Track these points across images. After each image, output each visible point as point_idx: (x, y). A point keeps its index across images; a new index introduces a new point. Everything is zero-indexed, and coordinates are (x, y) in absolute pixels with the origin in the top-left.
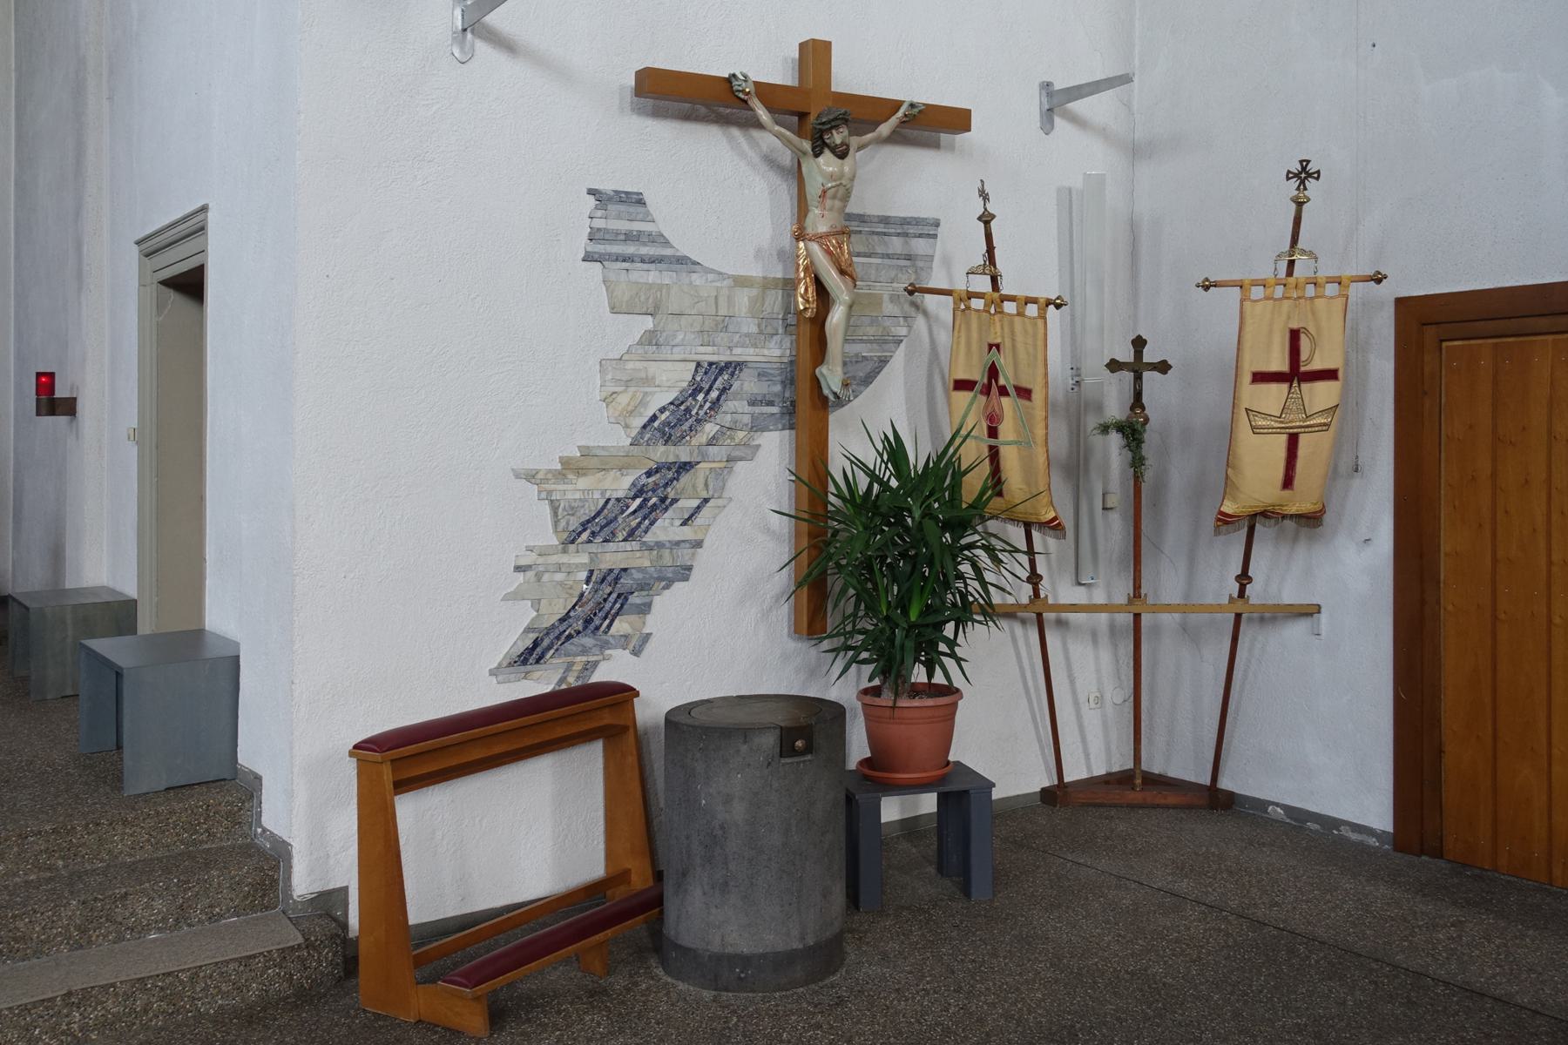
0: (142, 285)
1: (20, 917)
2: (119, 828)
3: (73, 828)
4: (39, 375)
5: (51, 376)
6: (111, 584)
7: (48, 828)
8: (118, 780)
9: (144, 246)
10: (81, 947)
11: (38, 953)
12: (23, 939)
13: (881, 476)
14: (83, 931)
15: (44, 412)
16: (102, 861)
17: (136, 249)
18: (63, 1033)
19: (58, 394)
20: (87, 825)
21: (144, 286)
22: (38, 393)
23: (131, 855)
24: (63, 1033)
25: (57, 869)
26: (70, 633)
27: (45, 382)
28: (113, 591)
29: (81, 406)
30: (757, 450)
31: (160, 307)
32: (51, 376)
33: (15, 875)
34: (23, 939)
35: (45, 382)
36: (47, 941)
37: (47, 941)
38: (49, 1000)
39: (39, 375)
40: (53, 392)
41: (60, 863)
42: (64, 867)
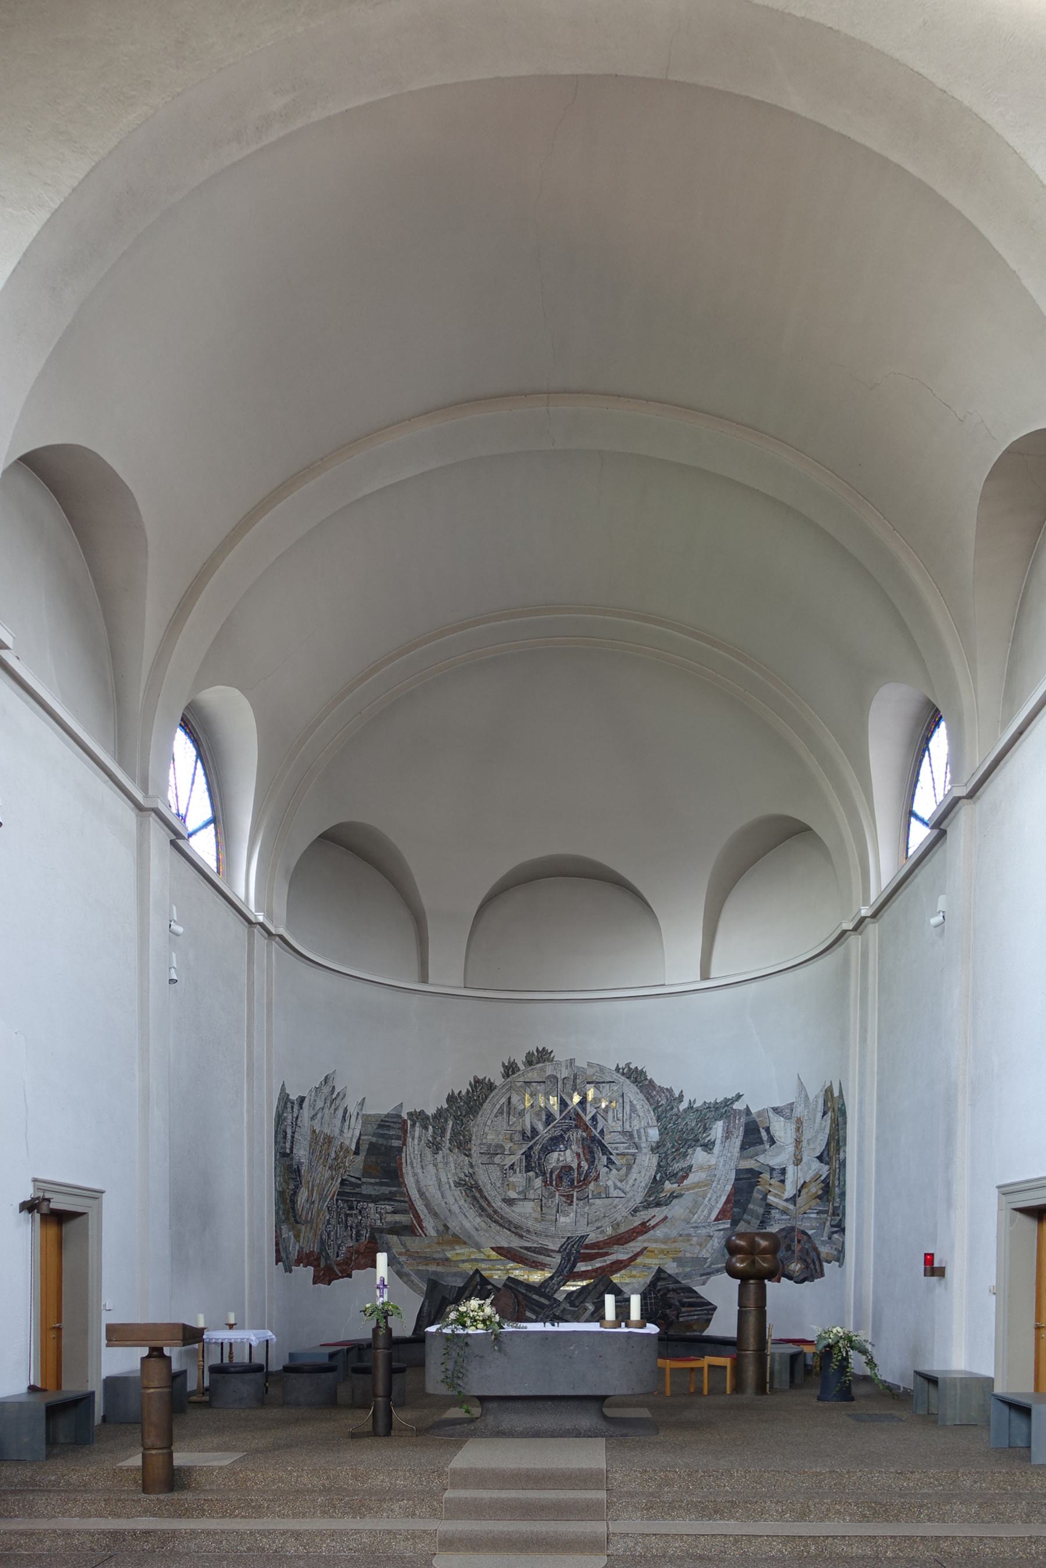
0: (1000, 1209)
1: (1001, 1504)
2: (1036, 1476)
3: (1015, 1473)
4: (926, 1255)
5: (932, 1255)
6: (968, 1369)
7: (1004, 1471)
8: (1028, 1458)
9: (1002, 1189)
10: (1026, 1523)
11: (1008, 1522)
12: (1002, 1514)
13: (681, 1315)
14: (1028, 1516)
15: (928, 1274)
16: (1028, 1490)
17: (996, 1191)
18: (1028, 1553)
19: (936, 1265)
20: (1021, 1473)
21: (1002, 1210)
22: (925, 1264)
23: (1041, 1490)
24: (1028, 1553)
25: (1007, 1490)
26: (959, 1392)
27: (929, 1259)
28: (971, 1373)
29: (948, 1272)
30: (576, 1437)
31: (1012, 1222)
32: (932, 1255)
33: (990, 1489)
34: (1002, 1514)
35: (929, 1259)
36: (1012, 1517)
37: (1012, 1517)
38: (1022, 1537)
39: (926, 1255)
40: (933, 1264)
41: (1009, 1488)
42: (1011, 1490)
